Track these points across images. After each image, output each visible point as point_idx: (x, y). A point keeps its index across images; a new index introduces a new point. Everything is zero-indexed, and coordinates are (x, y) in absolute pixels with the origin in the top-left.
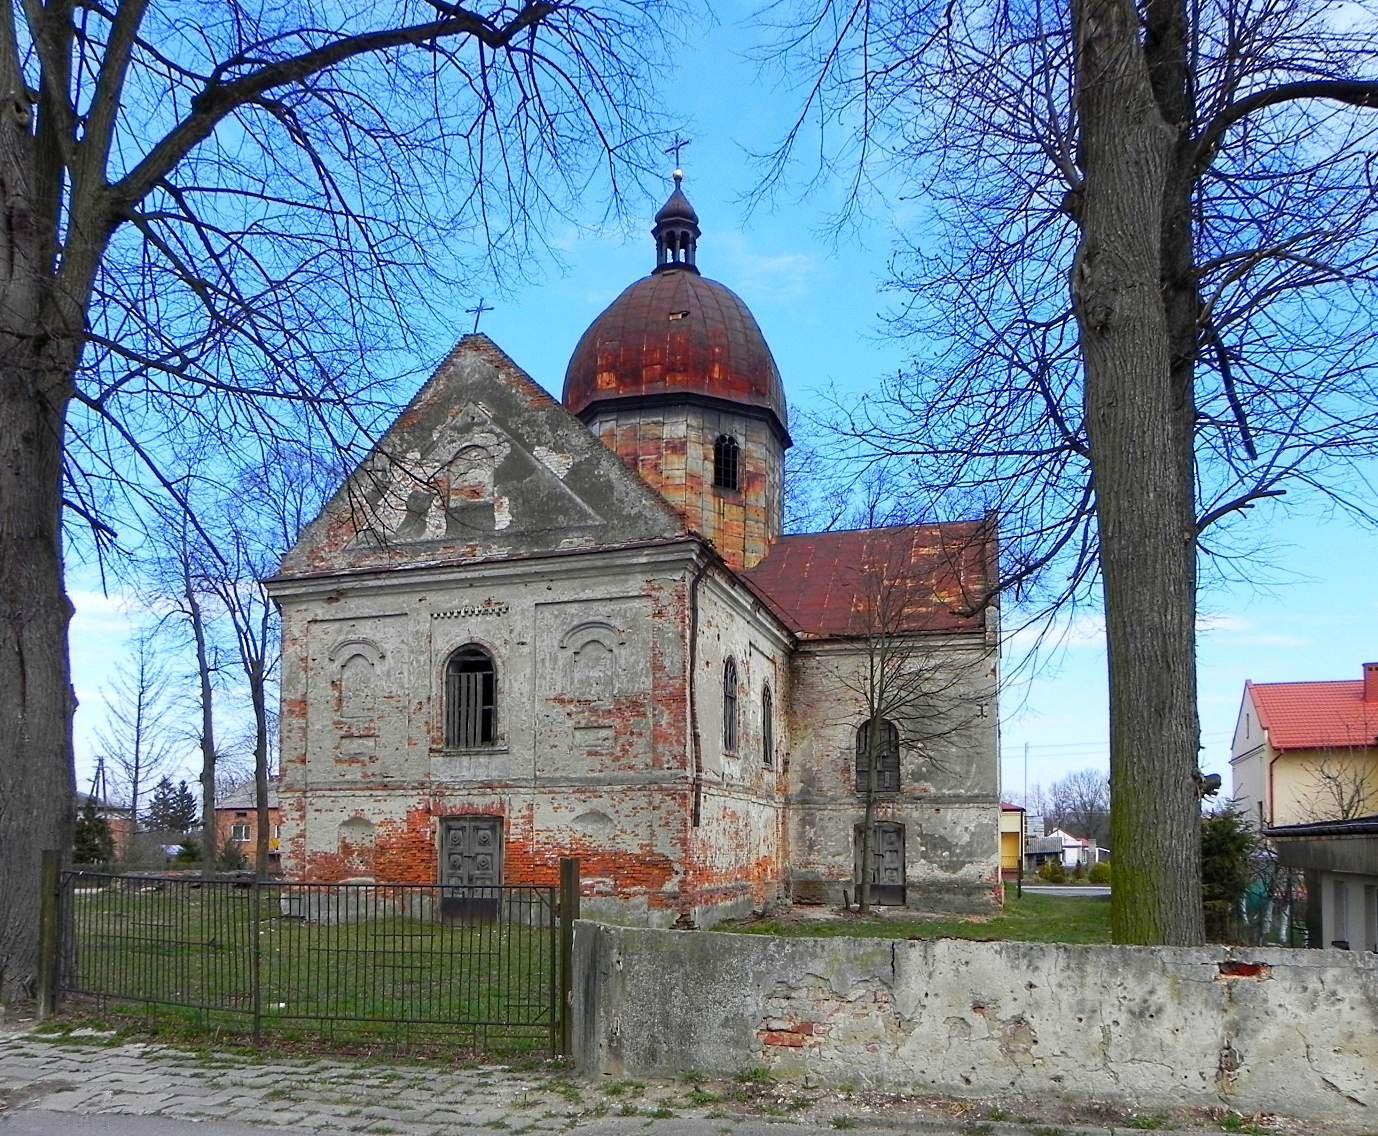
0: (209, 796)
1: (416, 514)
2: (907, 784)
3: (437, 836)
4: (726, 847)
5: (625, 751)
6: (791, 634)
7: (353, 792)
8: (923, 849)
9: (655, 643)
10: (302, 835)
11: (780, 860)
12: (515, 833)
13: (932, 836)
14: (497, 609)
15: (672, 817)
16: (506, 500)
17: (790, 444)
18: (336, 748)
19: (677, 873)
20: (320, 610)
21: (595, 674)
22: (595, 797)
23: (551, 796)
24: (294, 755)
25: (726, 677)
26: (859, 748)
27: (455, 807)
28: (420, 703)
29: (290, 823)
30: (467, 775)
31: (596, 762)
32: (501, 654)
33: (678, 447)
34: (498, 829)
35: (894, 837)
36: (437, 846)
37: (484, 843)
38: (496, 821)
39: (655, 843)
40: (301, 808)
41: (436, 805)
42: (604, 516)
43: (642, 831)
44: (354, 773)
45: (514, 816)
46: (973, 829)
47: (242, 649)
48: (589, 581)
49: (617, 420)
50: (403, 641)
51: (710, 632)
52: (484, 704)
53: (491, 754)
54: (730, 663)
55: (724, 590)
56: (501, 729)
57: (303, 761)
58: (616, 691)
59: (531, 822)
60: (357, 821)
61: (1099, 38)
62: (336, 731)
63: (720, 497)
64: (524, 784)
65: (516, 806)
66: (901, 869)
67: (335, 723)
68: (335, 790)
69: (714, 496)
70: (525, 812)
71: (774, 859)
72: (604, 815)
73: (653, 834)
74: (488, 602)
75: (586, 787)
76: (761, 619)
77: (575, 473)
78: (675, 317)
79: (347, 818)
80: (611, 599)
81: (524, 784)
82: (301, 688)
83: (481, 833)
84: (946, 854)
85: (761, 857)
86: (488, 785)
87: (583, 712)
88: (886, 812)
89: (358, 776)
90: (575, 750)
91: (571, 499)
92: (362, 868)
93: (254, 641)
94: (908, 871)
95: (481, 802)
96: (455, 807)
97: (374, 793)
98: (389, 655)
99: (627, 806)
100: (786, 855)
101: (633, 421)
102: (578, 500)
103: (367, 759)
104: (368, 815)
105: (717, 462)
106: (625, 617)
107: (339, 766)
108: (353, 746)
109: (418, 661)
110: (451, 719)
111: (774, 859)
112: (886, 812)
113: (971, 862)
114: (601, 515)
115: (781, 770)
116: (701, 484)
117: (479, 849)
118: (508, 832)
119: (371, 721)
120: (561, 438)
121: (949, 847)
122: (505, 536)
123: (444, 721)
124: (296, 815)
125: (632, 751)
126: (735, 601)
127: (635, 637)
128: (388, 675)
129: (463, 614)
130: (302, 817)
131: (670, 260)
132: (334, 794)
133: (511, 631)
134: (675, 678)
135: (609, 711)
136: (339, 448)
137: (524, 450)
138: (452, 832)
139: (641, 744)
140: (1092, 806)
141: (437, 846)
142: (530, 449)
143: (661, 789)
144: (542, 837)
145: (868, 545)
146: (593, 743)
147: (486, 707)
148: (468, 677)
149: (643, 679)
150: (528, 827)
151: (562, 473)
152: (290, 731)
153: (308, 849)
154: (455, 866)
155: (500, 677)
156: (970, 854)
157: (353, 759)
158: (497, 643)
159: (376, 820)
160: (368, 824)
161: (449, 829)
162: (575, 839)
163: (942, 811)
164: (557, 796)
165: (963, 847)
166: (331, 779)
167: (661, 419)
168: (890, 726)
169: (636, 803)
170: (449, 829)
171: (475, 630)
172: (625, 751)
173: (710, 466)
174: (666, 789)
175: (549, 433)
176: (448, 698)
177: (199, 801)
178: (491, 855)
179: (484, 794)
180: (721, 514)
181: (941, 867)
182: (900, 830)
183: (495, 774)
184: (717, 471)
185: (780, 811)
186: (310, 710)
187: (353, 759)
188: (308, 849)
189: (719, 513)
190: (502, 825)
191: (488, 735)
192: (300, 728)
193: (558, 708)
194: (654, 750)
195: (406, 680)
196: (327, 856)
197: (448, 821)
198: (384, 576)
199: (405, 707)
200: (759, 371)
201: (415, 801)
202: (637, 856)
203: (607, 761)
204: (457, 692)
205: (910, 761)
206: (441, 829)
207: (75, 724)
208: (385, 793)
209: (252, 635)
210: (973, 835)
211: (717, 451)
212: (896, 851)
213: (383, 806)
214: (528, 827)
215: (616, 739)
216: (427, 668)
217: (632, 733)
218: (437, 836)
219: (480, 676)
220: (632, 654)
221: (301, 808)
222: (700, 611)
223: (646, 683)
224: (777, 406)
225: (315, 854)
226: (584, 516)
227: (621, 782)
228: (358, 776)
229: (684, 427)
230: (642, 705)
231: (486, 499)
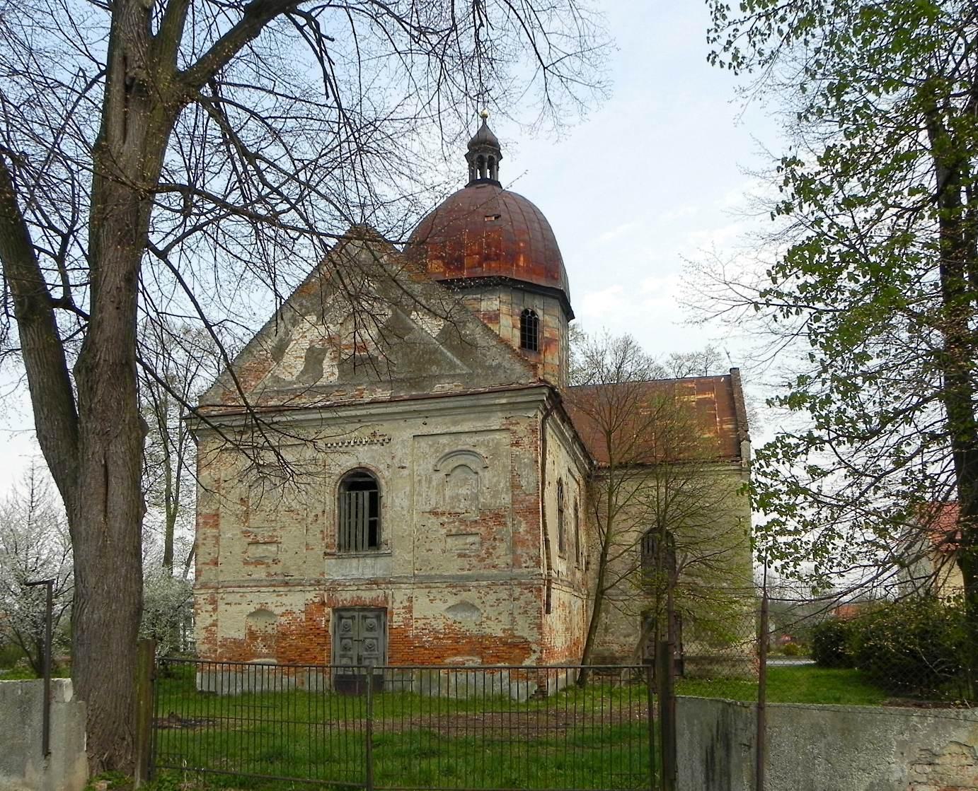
7: (259, 589)
10: (215, 624)
14: (381, 439)
23: (428, 590)
27: (346, 600)
29: (204, 615)
30: (356, 574)
38: (381, 611)
40: (213, 602)
44: (260, 573)
48: (459, 417)
53: (377, 556)
59: (411, 612)
60: (262, 612)
62: (244, 539)
67: (243, 532)
68: (244, 587)
72: (473, 606)
74: (374, 435)
75: (457, 583)
80: (476, 432)
81: (405, 580)
86: (374, 582)
89: (263, 575)
95: (368, 596)
96: (346, 600)
97: (276, 589)
104: (272, 607)
108: (259, 551)
124: (210, 608)
131: (479, 177)
138: (343, 621)
143: (520, 584)
152: (205, 539)
153: (219, 637)
157: (259, 562)
159: (278, 611)
160: (271, 614)
161: (341, 618)
164: (433, 591)
170: (341, 618)
178: (377, 639)
179: (371, 589)
186: (222, 521)
187: (259, 562)
194: (514, 552)
197: (340, 611)
200: (551, 262)
202: (500, 639)
208: (286, 589)
213: (284, 600)
221: (213, 602)
225: (226, 639)
226: (453, 366)
227: (487, 578)
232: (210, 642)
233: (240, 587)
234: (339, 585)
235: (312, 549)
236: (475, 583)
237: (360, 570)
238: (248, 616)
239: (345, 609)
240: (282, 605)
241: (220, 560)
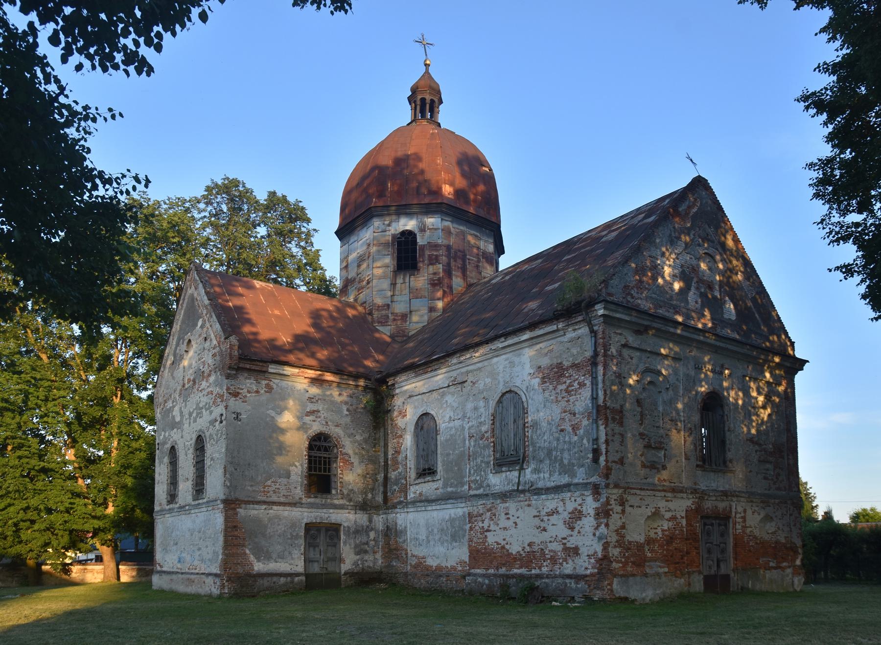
10: (623, 527)
20: (632, 339)
30: (714, 485)
40: (622, 502)
60: (656, 514)
68: (644, 489)
70: (743, 515)
79: (650, 514)
92: (649, 555)
95: (721, 505)
96: (708, 508)
103: (660, 466)
104: (662, 510)
124: (619, 509)
130: (623, 512)
132: (643, 493)
145: (146, 327)
153: (628, 538)
161: (705, 524)
179: (723, 500)
188: (628, 538)
198: (691, 330)
207: (796, 382)
213: (671, 505)
221: (622, 502)
225: (630, 543)
232: (621, 547)
233: (641, 489)
234: (706, 494)
236: (773, 501)
238: (646, 520)
240: (670, 510)
241: (625, 461)
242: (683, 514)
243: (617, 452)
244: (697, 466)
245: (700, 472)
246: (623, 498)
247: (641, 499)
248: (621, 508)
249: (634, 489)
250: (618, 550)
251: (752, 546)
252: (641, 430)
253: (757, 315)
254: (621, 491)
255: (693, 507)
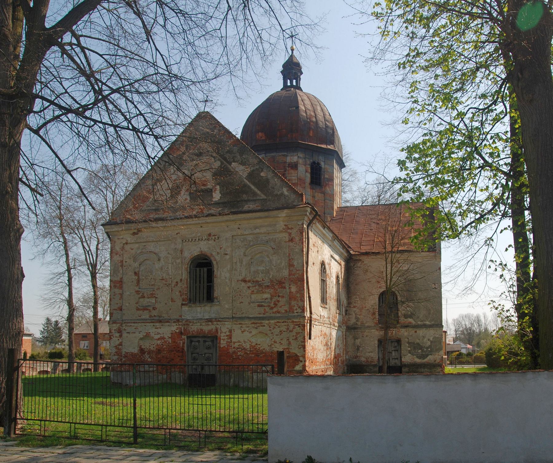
0: (71, 329)
1: (175, 191)
2: (402, 320)
3: (185, 345)
4: (322, 349)
5: (276, 305)
6: (348, 252)
7: (145, 324)
8: (409, 349)
9: (289, 254)
10: (121, 344)
11: (344, 355)
12: (223, 343)
13: (414, 343)
14: (213, 238)
15: (298, 335)
16: (218, 187)
17: (344, 166)
18: (137, 303)
19: (301, 361)
21: (261, 268)
22: (262, 326)
23: (241, 325)
24: (116, 307)
25: (321, 271)
26: (379, 304)
28: (177, 282)
30: (199, 316)
31: (262, 309)
32: (216, 259)
33: (294, 166)
34: (215, 341)
35: (396, 344)
36: (185, 349)
37: (208, 348)
38: (214, 338)
39: (290, 347)
41: (185, 330)
42: (265, 195)
43: (285, 342)
44: (145, 315)
45: (223, 337)
46: (431, 339)
47: (86, 259)
49: (265, 154)
50: (168, 253)
51: (315, 249)
52: (208, 283)
54: (323, 264)
55: (320, 230)
56: (216, 294)
57: (121, 310)
58: (271, 276)
59: (231, 338)
61: (172, 174)
63: (313, 189)
64: (227, 320)
65: (224, 329)
66: (399, 359)
68: (136, 323)
69: (311, 188)
70: (228, 333)
71: (342, 355)
73: (290, 343)
76: (336, 244)
77: (251, 176)
78: (292, 109)
79: (142, 336)
82: (120, 276)
83: (207, 343)
84: (420, 351)
85: (336, 354)
86: (210, 320)
87: (255, 286)
88: (394, 333)
89: (148, 317)
90: (251, 304)
91: (249, 187)
93: (92, 255)
94: (403, 360)
95: (207, 328)
96: (194, 331)
97: (154, 324)
98: (162, 259)
99: (277, 330)
100: (347, 353)
101: (273, 154)
102: (253, 187)
103: (151, 308)
104: (152, 335)
105: (312, 173)
106: (275, 242)
107: (138, 312)
109: (176, 263)
110: (192, 291)
111: (342, 355)
112: (394, 333)
113: (431, 355)
114: (264, 194)
115: (344, 314)
116: (305, 183)
117: (206, 351)
118: (220, 343)
119: (154, 291)
120: (245, 159)
121: (421, 348)
122: (217, 204)
123: (189, 291)
124: (118, 335)
125: (280, 304)
126: (324, 235)
127: (280, 251)
128: (162, 269)
129: (197, 240)
130: (121, 336)
131: (289, 84)
132: (136, 325)
133: (221, 248)
134: (299, 270)
135: (268, 286)
136: (149, 156)
137: (227, 164)
138: (193, 343)
139: (282, 301)
140: (470, 330)
141: (185, 349)
142: (230, 163)
144: (236, 345)
146: (260, 301)
147: (208, 284)
148: (200, 269)
149: (284, 271)
150: (229, 340)
151: (245, 175)
153: (124, 351)
154: (195, 359)
155: (215, 270)
156: (431, 351)
157: (145, 309)
158: (214, 254)
161: (191, 342)
162: (252, 346)
163: (418, 331)
165: (427, 348)
166: (134, 318)
167: (286, 153)
168: (394, 294)
169: (281, 329)
170: (191, 342)
171: (204, 247)
172: (276, 305)
173: (309, 175)
174: (296, 322)
175: (239, 157)
176: (190, 280)
177: (66, 331)
178: (212, 354)
179: (209, 325)
180: (314, 197)
181: (417, 357)
182: (399, 341)
183: (213, 316)
184: (312, 177)
185: (344, 333)
186: (124, 286)
187: (145, 309)
188: (124, 351)
189: (313, 197)
190: (217, 339)
191: (210, 297)
192: (120, 294)
193: (243, 284)
194: (290, 304)
195: (170, 271)
196: (132, 354)
197: (191, 338)
199: (169, 284)
201: (174, 328)
203: (267, 309)
204: (194, 277)
205: (402, 310)
206: (187, 342)
208: (160, 324)
209: (91, 253)
210: (431, 342)
211: (312, 168)
212: (397, 351)
213: (159, 330)
214: (229, 340)
215: (271, 299)
216: (180, 265)
217: (279, 296)
218: (185, 345)
219: (205, 269)
220: (278, 259)
222: (310, 239)
223: (286, 273)
224: (338, 149)
225: (127, 353)
226: (255, 194)
228: (148, 317)
229: (297, 157)
230: (284, 283)
231: (209, 186)
232: (118, 355)
233: (134, 323)
234: (190, 322)
235: (175, 301)
237: (202, 314)
239: (195, 337)
240: (158, 334)
241: (123, 307)
242: (170, 336)
243: (117, 304)
244: (182, 304)
245: (187, 308)
246: (120, 329)
247: (135, 328)
248: (119, 334)
249: (129, 323)
250: (116, 357)
251: (240, 355)
252: (137, 289)
253: (253, 187)
254: (118, 325)
255: (177, 331)
